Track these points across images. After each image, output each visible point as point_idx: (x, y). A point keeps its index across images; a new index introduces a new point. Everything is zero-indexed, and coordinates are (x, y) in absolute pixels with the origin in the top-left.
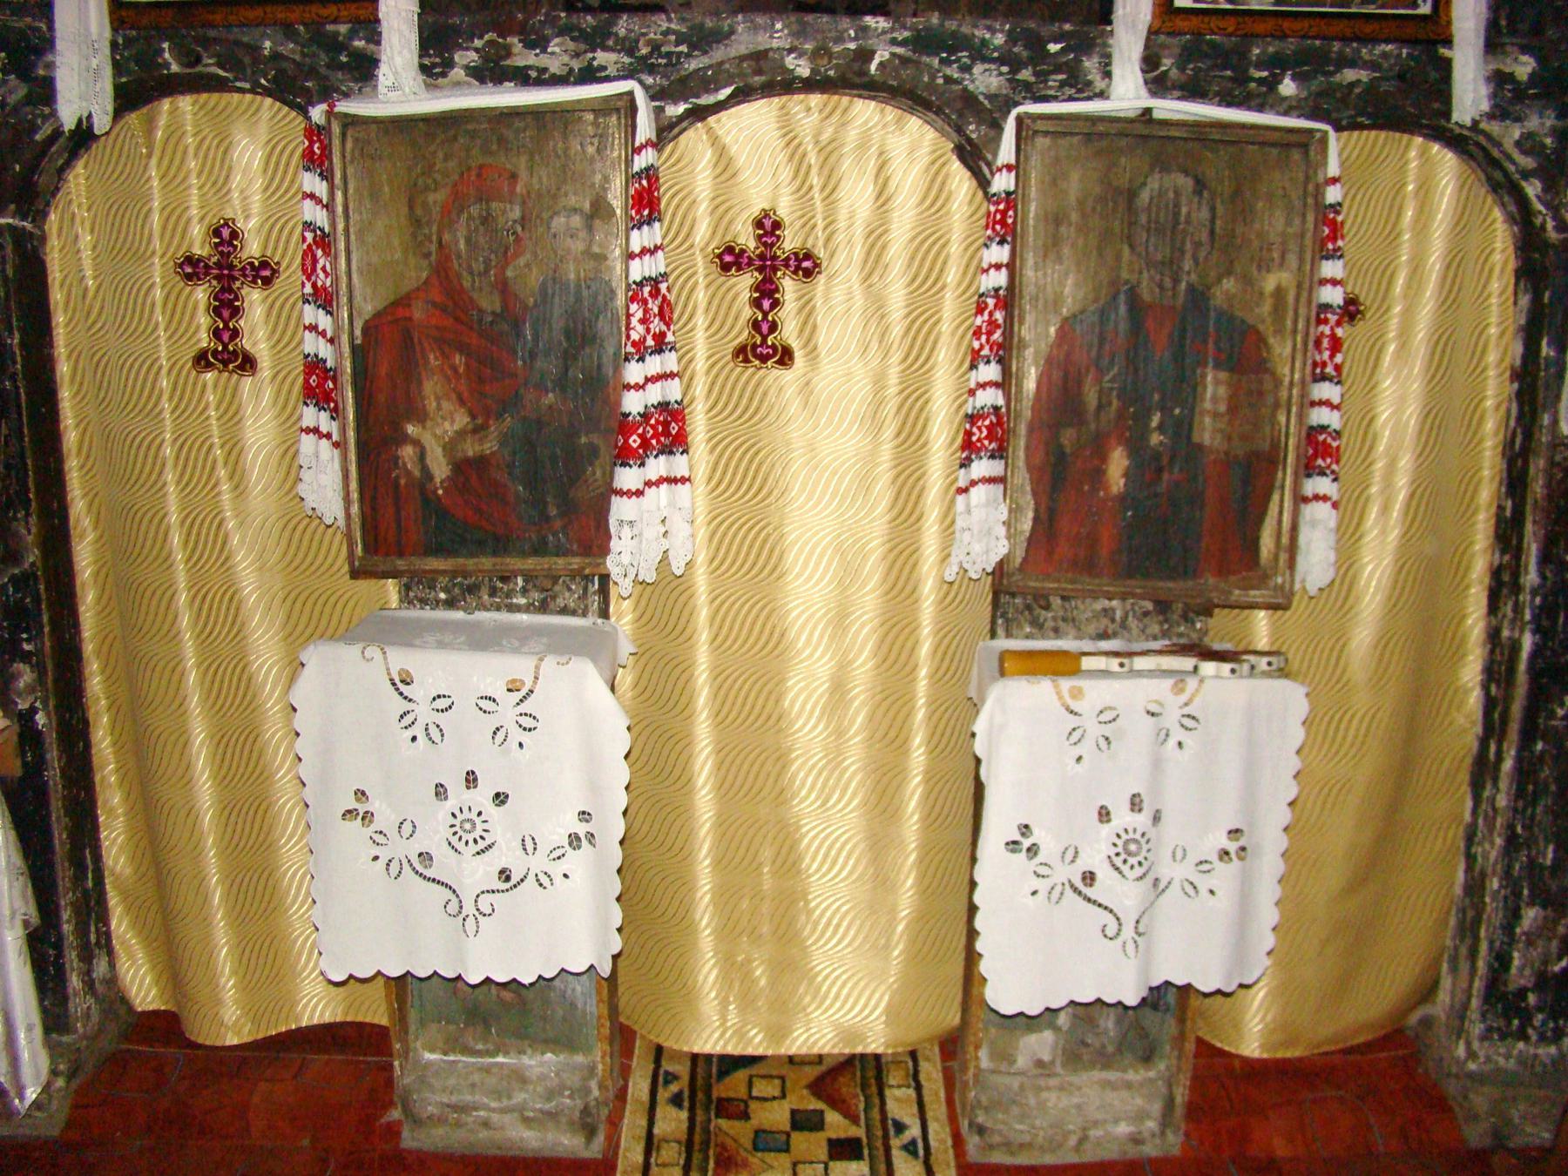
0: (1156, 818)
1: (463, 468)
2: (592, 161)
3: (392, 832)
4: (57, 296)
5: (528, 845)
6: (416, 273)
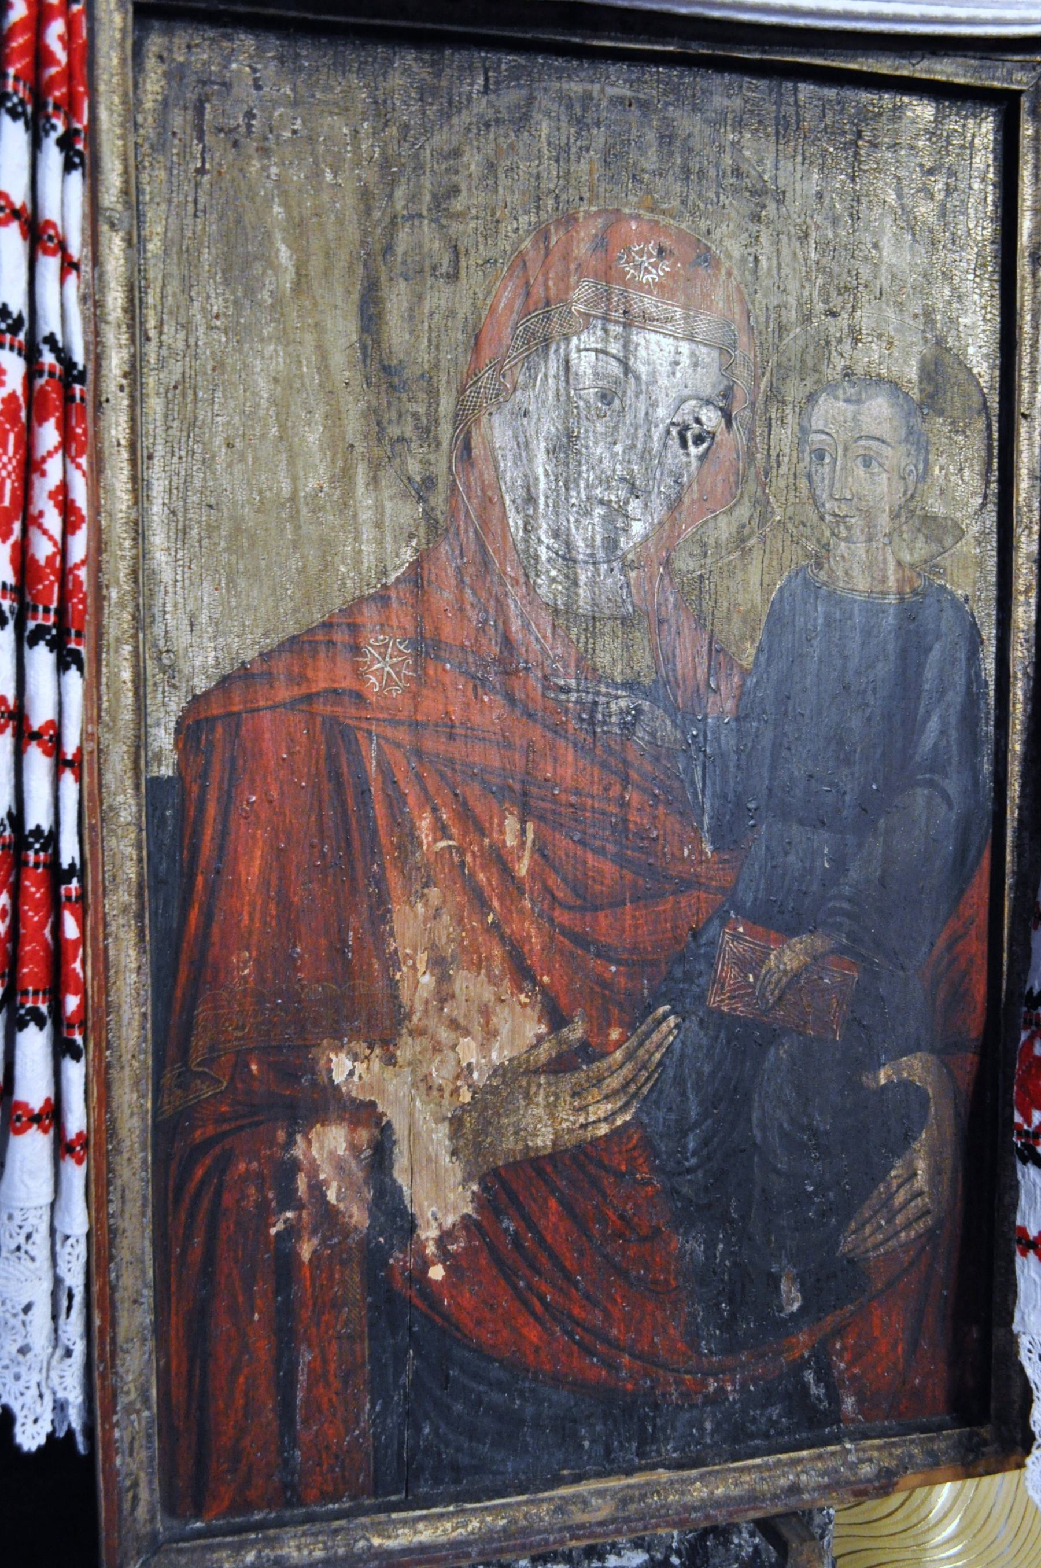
1: (507, 1186)
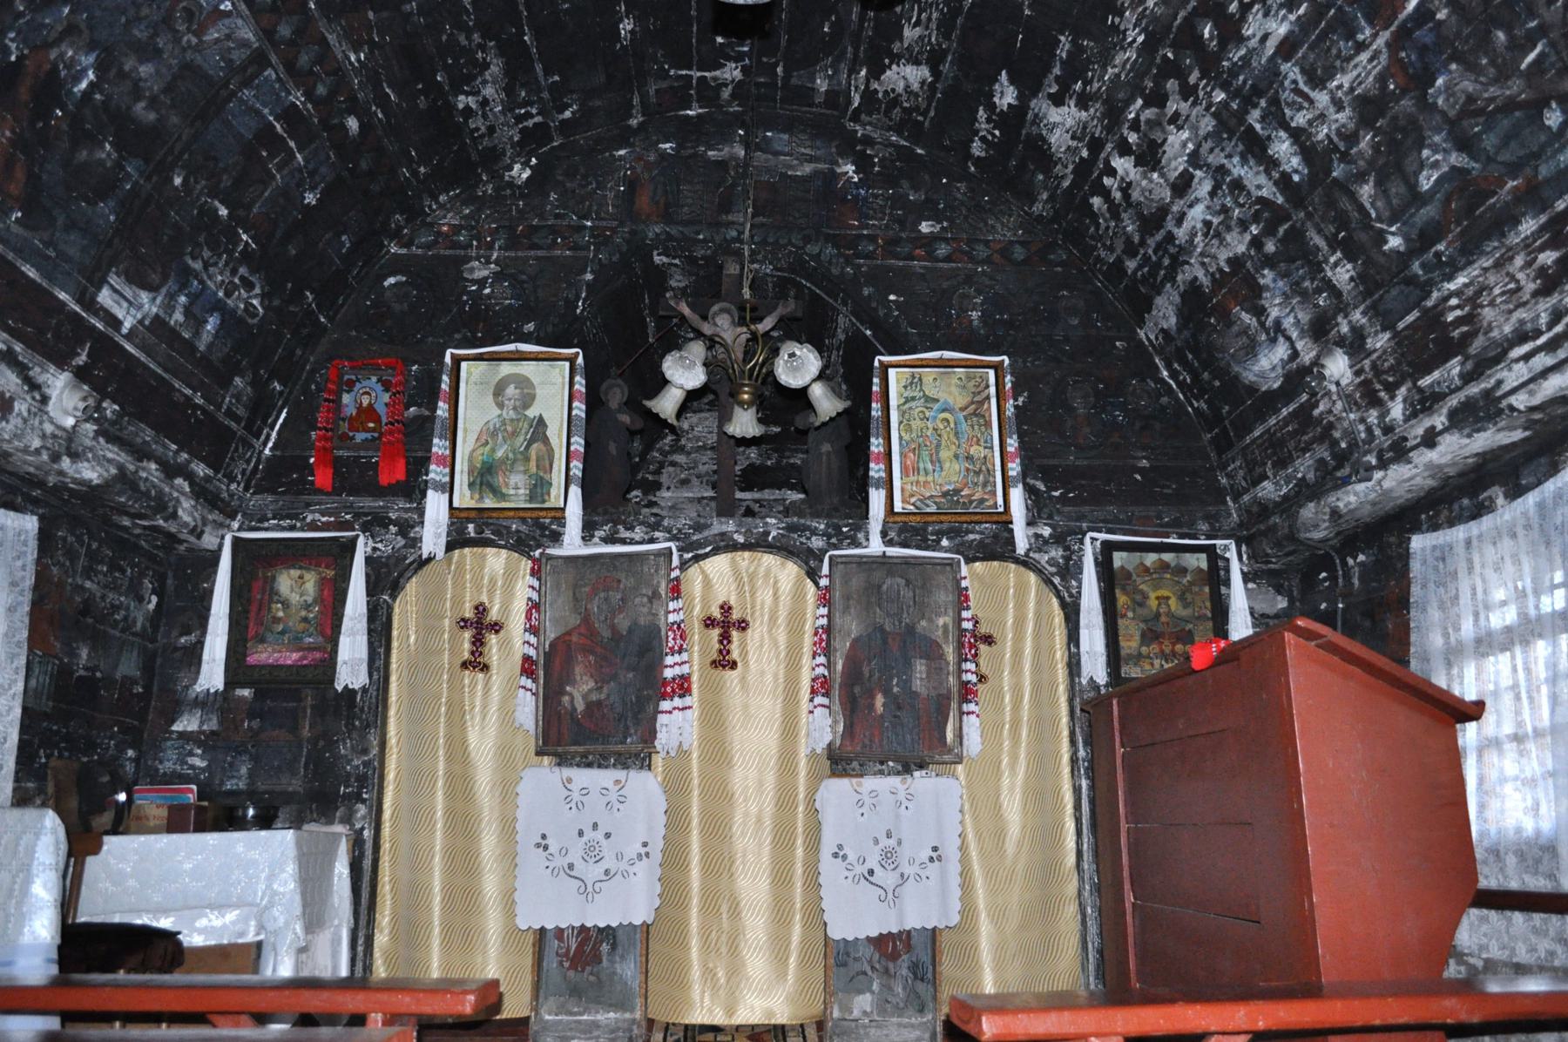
0: (899, 843)
1: (592, 707)
4: (395, 633)
5: (619, 856)
6: (574, 620)
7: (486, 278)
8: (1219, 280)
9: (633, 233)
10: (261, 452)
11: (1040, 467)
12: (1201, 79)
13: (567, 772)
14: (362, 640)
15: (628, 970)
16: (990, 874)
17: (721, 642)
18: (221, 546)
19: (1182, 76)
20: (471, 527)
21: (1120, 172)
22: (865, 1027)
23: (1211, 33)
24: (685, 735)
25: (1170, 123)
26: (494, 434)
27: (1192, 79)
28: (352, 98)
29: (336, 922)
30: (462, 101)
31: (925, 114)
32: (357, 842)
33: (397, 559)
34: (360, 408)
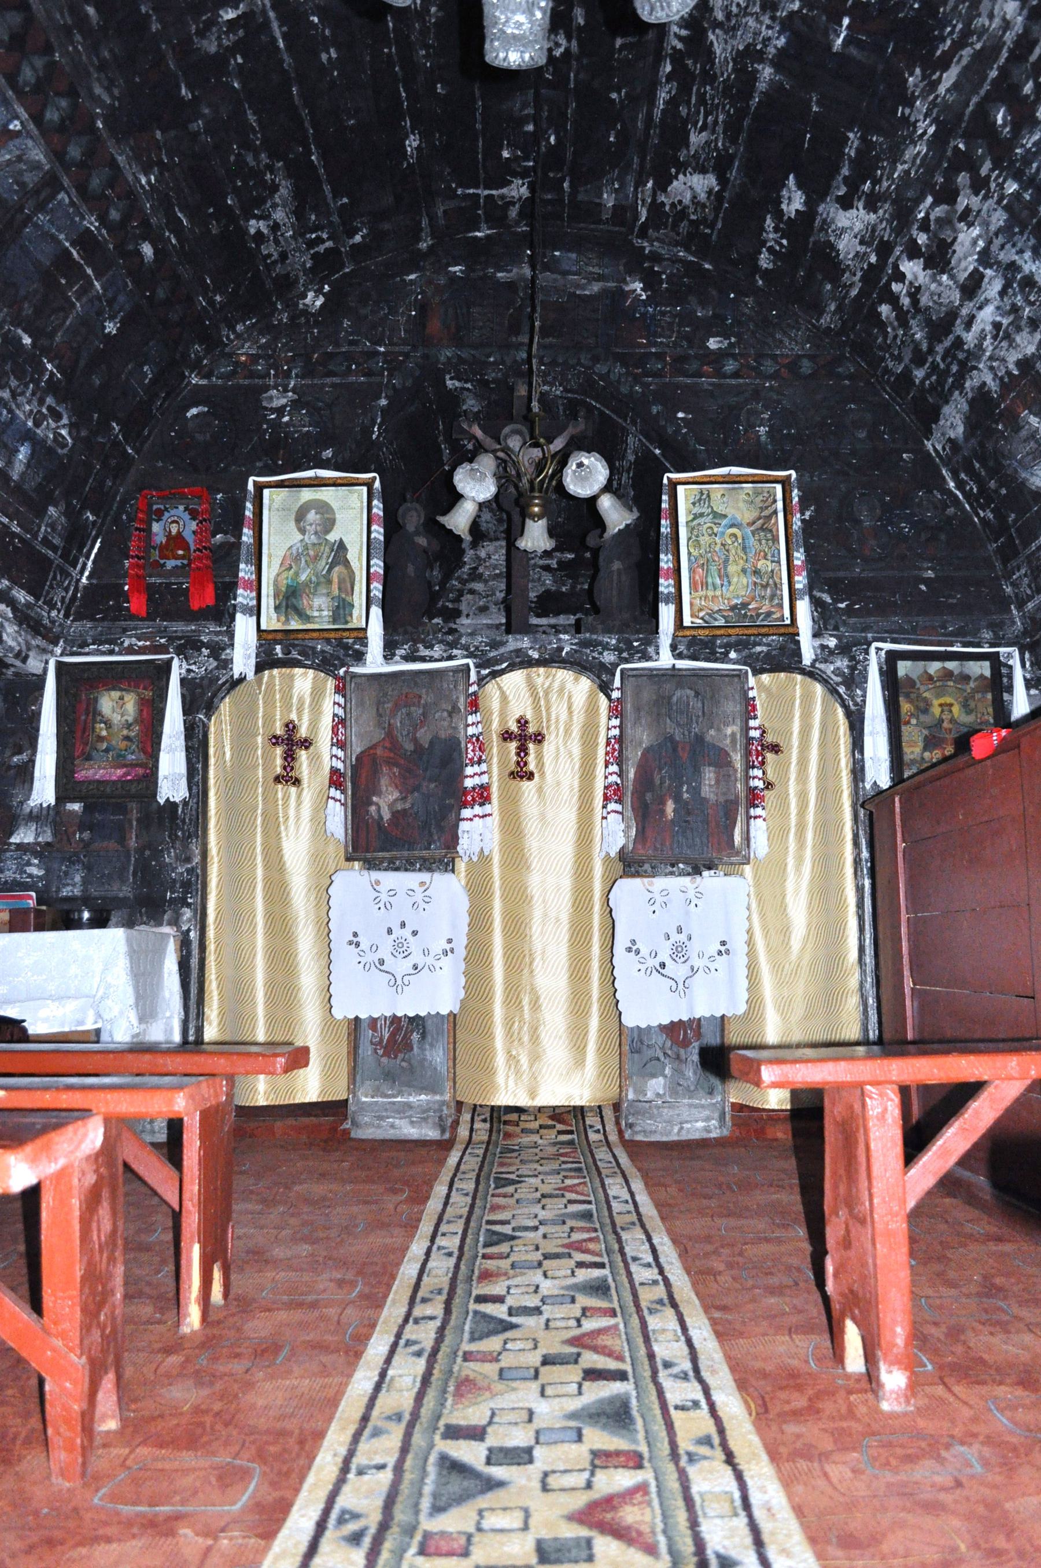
1: (395, 814)
2: (451, 690)
3: (367, 950)
4: (211, 751)
5: (426, 952)
6: (379, 735)
7: (284, 407)
8: (1008, 383)
9: (425, 357)
10: (78, 581)
11: (821, 576)
12: (992, 170)
13: (375, 875)
14: (181, 757)
15: (437, 1056)
16: (777, 968)
17: (518, 754)
18: (45, 671)
19: (973, 168)
20: (278, 648)
21: (909, 276)
22: (658, 1107)
23: (1004, 118)
24: (486, 841)
25: (960, 220)
26: (297, 559)
27: (984, 171)
28: (145, 223)
29: (168, 1014)
30: (254, 226)
31: (712, 226)
32: (185, 943)
33: (210, 680)
34: (169, 536)
